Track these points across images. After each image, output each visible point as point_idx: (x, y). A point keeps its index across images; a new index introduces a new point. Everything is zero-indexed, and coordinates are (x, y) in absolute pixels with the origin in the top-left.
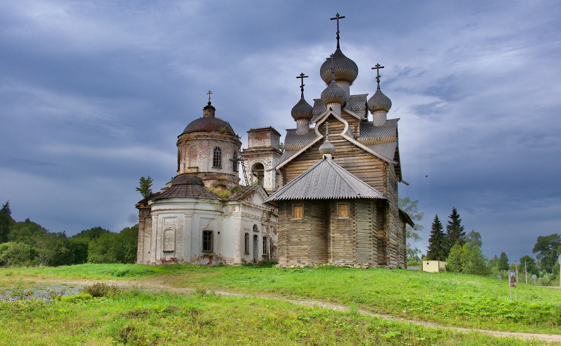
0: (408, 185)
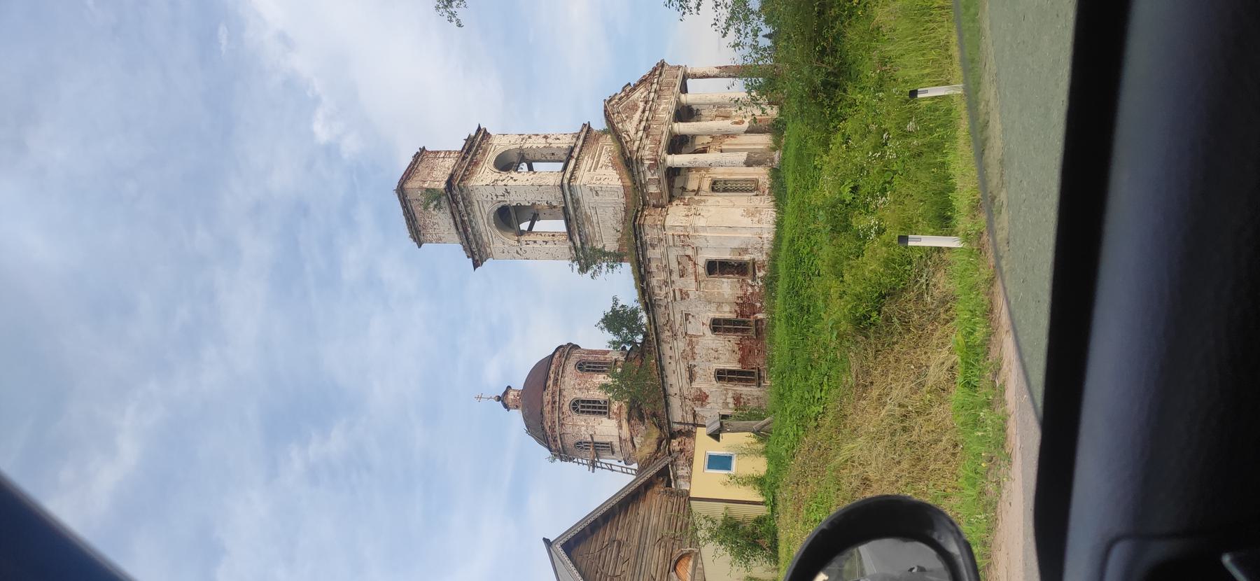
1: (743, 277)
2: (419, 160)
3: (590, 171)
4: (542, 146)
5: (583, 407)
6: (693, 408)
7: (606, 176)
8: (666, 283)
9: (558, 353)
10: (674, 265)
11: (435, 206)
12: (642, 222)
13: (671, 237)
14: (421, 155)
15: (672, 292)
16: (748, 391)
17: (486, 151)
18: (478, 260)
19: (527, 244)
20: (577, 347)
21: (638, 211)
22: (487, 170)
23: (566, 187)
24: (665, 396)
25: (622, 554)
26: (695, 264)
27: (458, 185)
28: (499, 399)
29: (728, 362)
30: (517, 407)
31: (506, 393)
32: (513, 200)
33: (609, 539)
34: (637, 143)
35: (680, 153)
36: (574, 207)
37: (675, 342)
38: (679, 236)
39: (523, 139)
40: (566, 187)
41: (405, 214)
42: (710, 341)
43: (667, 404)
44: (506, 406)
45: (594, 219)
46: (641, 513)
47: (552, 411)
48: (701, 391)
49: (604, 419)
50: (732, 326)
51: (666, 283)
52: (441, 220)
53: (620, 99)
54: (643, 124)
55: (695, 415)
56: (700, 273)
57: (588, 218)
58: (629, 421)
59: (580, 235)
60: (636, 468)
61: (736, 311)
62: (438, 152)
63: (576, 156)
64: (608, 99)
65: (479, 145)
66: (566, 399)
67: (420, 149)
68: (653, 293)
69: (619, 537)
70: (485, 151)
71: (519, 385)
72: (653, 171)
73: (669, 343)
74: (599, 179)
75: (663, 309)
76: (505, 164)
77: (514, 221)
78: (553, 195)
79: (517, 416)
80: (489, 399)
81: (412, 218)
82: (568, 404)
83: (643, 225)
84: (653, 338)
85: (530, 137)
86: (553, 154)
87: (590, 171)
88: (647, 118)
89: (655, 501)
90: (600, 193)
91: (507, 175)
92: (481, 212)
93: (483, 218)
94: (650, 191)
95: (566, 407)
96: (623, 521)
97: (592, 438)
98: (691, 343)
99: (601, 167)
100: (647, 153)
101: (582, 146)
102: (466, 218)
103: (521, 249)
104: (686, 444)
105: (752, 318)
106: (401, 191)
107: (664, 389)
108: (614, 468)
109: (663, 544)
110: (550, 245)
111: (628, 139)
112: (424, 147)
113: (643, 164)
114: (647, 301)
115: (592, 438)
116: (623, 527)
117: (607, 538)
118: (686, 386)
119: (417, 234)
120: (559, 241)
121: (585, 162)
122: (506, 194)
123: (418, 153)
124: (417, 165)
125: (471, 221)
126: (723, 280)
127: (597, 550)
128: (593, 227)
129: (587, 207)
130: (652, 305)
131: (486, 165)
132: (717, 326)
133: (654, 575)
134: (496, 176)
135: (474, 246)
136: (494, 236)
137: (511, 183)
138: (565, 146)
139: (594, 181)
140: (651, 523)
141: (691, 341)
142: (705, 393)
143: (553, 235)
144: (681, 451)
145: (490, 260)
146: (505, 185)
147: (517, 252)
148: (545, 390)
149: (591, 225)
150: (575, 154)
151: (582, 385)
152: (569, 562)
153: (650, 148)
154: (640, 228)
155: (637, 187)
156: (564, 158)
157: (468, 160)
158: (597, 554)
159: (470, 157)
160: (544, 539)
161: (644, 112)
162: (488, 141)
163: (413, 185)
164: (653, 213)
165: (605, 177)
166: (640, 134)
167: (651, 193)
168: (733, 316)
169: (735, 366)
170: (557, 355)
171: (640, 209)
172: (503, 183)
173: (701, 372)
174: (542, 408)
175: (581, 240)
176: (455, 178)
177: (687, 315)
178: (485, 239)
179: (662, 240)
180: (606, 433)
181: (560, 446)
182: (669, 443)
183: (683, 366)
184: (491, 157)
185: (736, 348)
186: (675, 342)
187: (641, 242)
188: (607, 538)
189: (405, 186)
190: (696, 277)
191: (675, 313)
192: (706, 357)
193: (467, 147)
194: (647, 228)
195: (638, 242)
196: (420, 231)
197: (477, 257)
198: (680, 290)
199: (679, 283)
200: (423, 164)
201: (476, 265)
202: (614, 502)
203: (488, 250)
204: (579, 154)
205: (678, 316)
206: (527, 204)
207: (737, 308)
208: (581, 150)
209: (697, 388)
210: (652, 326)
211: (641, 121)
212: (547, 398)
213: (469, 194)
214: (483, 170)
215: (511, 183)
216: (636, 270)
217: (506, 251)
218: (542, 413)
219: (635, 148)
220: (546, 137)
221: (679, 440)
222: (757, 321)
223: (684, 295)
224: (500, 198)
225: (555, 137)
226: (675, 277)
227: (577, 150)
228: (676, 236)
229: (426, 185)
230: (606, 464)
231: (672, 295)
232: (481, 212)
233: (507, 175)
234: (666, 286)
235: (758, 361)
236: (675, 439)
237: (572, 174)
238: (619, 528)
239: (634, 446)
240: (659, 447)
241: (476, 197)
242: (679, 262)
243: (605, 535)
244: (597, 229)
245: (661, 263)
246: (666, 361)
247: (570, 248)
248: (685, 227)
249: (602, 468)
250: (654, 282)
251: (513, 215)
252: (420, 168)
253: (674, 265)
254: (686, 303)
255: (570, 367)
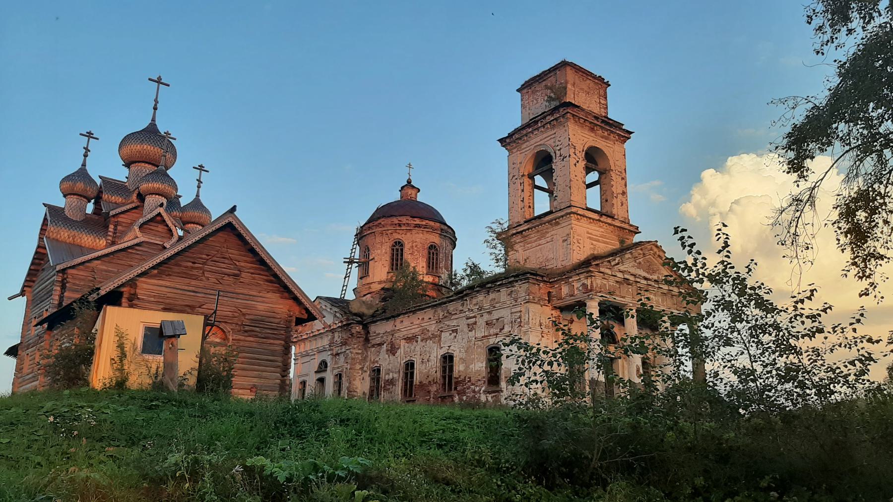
0: (10, 299)
1: (486, 382)
2: (597, 81)
3: (588, 233)
4: (614, 189)
5: (397, 250)
6: (385, 342)
7: (582, 247)
8: (480, 309)
9: (446, 228)
10: (496, 315)
11: (550, 97)
12: (530, 281)
13: (519, 309)
14: (602, 83)
15: (473, 315)
16: (398, 388)
17: (606, 139)
18: (505, 142)
19: (521, 184)
20: (454, 247)
21: (542, 276)
22: (586, 140)
23: (569, 211)
24: (393, 317)
25: (226, 278)
26: (497, 334)
27: (568, 112)
28: (409, 182)
29: (420, 373)
30: (401, 197)
31: (413, 187)
32: (557, 165)
33: (242, 266)
34: (608, 272)
35: (638, 325)
36: (552, 220)
37: (434, 322)
38: (520, 317)
39: (621, 172)
40: (569, 211)
41: (544, 72)
42: (436, 354)
43: (387, 319)
44: (402, 188)
45: (543, 241)
46: (269, 295)
47: (392, 224)
48: (398, 349)
49: (387, 269)
50: (447, 373)
51: (480, 309)
52: (540, 105)
53: (659, 256)
54: (632, 278)
55: (380, 345)
56: (490, 340)
57: (543, 236)
58: (383, 289)
59: (528, 229)
60: (345, 298)
61: (460, 376)
62: (606, 98)
63: (602, 219)
64: (659, 244)
65: (612, 132)
66: (403, 235)
67: (608, 82)
68: (472, 298)
69: (243, 275)
70: (607, 138)
71: (420, 198)
72: (581, 288)
73: (434, 316)
74: (579, 241)
75: (461, 308)
76: (593, 158)
77: (540, 170)
78: (563, 201)
79: (396, 196)
80: (409, 174)
81: (540, 79)
82: (399, 237)
83: (528, 282)
84: (436, 301)
85: (623, 179)
86: (607, 201)
87: (588, 233)
88: (639, 282)
89: (282, 307)
90: (565, 244)
91: (580, 157)
92: (546, 138)
93: (541, 140)
94: (562, 287)
95: (396, 236)
96: (260, 279)
97: (372, 260)
98: (434, 336)
99: (592, 244)
100: (598, 281)
101: (614, 226)
102: (539, 125)
103: (516, 179)
104: (358, 339)
105: (453, 392)
106: (564, 64)
107: (399, 315)
108: (347, 279)
109: (236, 314)
110: (521, 204)
111: (613, 263)
112: (609, 85)
113: (587, 278)
114: (465, 293)
115: (372, 260)
116: (254, 278)
117: (242, 264)
118: (401, 334)
119: (527, 87)
120: (524, 212)
121: (598, 229)
122: (562, 158)
123: (604, 79)
124: (591, 78)
125: (537, 129)
126: (484, 363)
127: (230, 255)
128: (536, 241)
129: (553, 233)
130: (462, 297)
131: (592, 138)
132: (448, 359)
133: (204, 307)
134: (579, 147)
135: (517, 136)
136: (526, 153)
137: (573, 161)
138: (615, 211)
139: (576, 237)
140: (258, 304)
141: (436, 338)
142: (396, 352)
143: (530, 207)
144: (352, 334)
145: (507, 153)
146: (570, 155)
147: (514, 176)
148: (411, 217)
149: (538, 238)
150: (604, 219)
151: (416, 249)
152: (214, 229)
153: (605, 285)
154: (525, 279)
155: (565, 275)
156: (604, 211)
157: (595, 122)
158: (227, 255)
159: (599, 123)
160: (235, 207)
161: (646, 279)
162: (617, 141)
163: (570, 73)
164: (542, 291)
165: (582, 247)
166: (620, 275)
167: (561, 289)
168: (455, 374)
169: (417, 378)
170: (443, 227)
171: (545, 279)
172: (572, 154)
173: (413, 348)
174: (395, 216)
175: (525, 230)
176: (575, 110)
177: (456, 331)
178: (524, 146)
179: (516, 301)
180: (375, 271)
181: (365, 234)
182: (359, 323)
183: (416, 330)
184: (600, 144)
185: (430, 379)
186: (434, 322)
187: (513, 281)
188: (242, 264)
189: (568, 68)
190: (487, 336)
191: (458, 320)
192: (423, 351)
193: (611, 122)
194: (526, 285)
195: (512, 279)
196: (530, 88)
197: (508, 141)
198: (476, 322)
199: (481, 322)
200: (592, 84)
201: (501, 141)
202: (276, 270)
203: (514, 151)
204: (606, 223)
205: (454, 323)
206: (554, 178)
207: (462, 377)
208: (610, 224)
209: (400, 345)
210: (445, 300)
211: (635, 276)
212: (404, 220)
213: (561, 124)
214: (585, 135)
215: (573, 161)
216: (489, 280)
217: (515, 166)
218: (392, 216)
219: (602, 270)
220: (624, 193)
221: (362, 333)
222: (452, 397)
223: (471, 327)
224: (558, 152)
225: (624, 201)
226: (486, 317)
227: (609, 220)
228: (519, 314)
229: (569, 86)
230: (350, 272)
231: (471, 315)
232: (546, 138)
233: (580, 157)
234: (478, 309)
235: (420, 397)
236: (363, 329)
237: (583, 216)
238: (253, 275)
239: (365, 295)
240: (355, 314)
241: (559, 131)
242: (498, 319)
243: (245, 263)
244: (534, 244)
245: (497, 303)
246: (420, 314)
247: (518, 222)
248: (528, 323)
249: (347, 270)
250: (481, 297)
251: (545, 168)
252: (588, 81)
253: (496, 315)
254: (466, 329)
255: (435, 239)
